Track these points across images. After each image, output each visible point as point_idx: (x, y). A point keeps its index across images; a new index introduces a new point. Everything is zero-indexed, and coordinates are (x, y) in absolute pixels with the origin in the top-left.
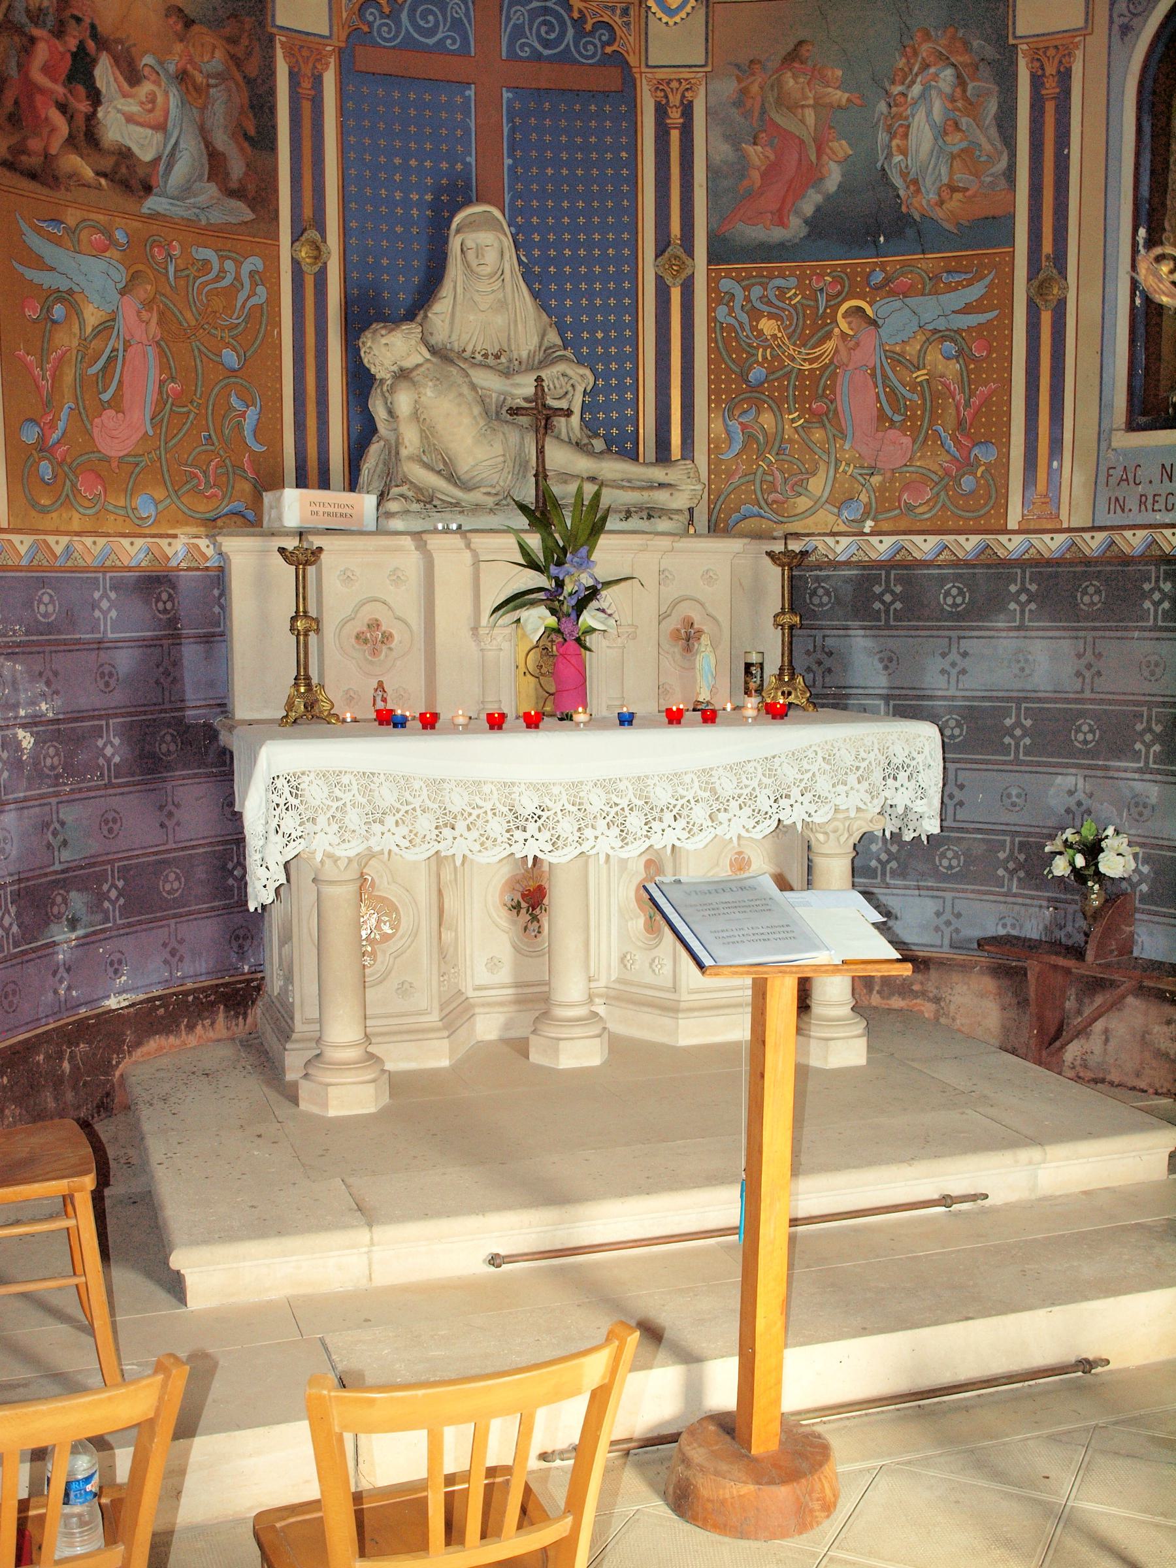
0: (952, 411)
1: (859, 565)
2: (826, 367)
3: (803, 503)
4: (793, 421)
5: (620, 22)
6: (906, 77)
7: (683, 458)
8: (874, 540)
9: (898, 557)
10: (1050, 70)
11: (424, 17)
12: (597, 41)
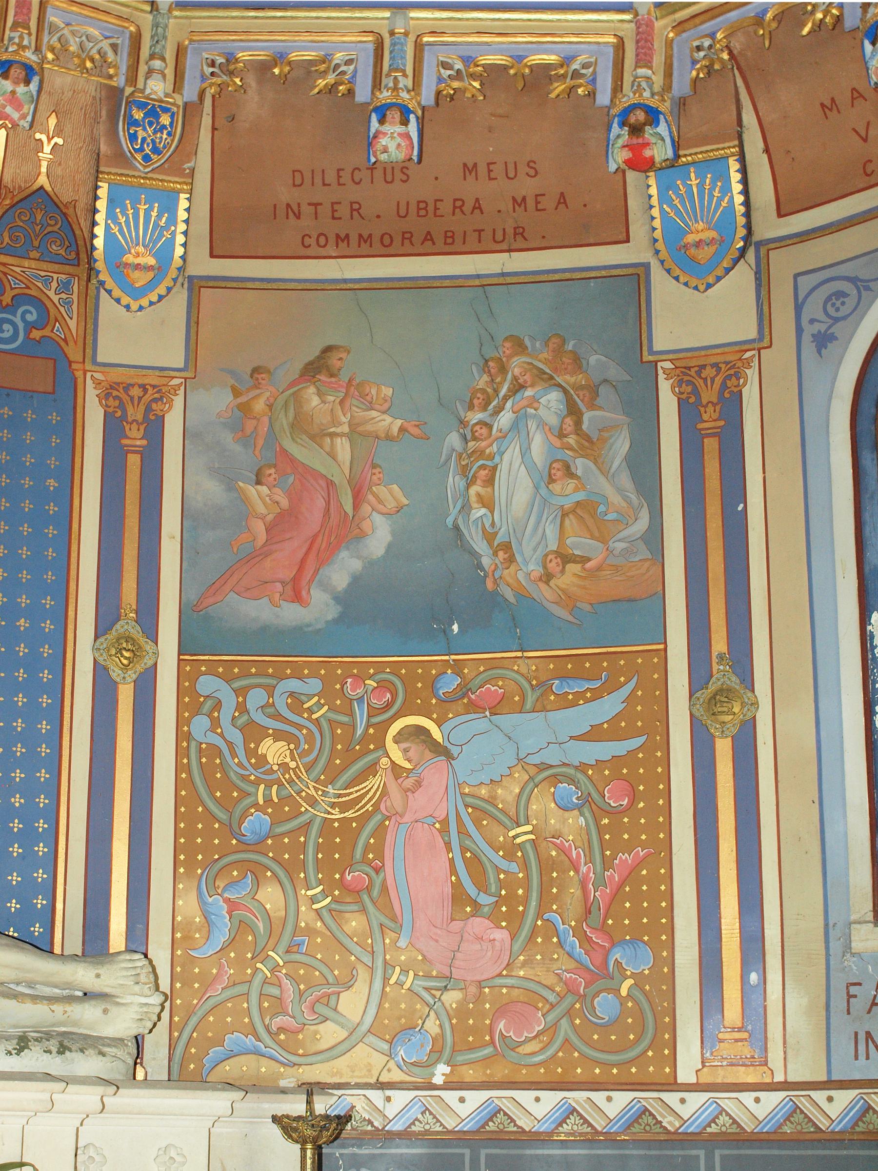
0: (574, 890)
1: (424, 1137)
2: (368, 816)
3: (330, 1033)
4: (313, 900)
5: (55, 299)
6: (486, 400)
7: (129, 950)
8: (451, 1097)
9: (492, 1126)
12: (18, 320)
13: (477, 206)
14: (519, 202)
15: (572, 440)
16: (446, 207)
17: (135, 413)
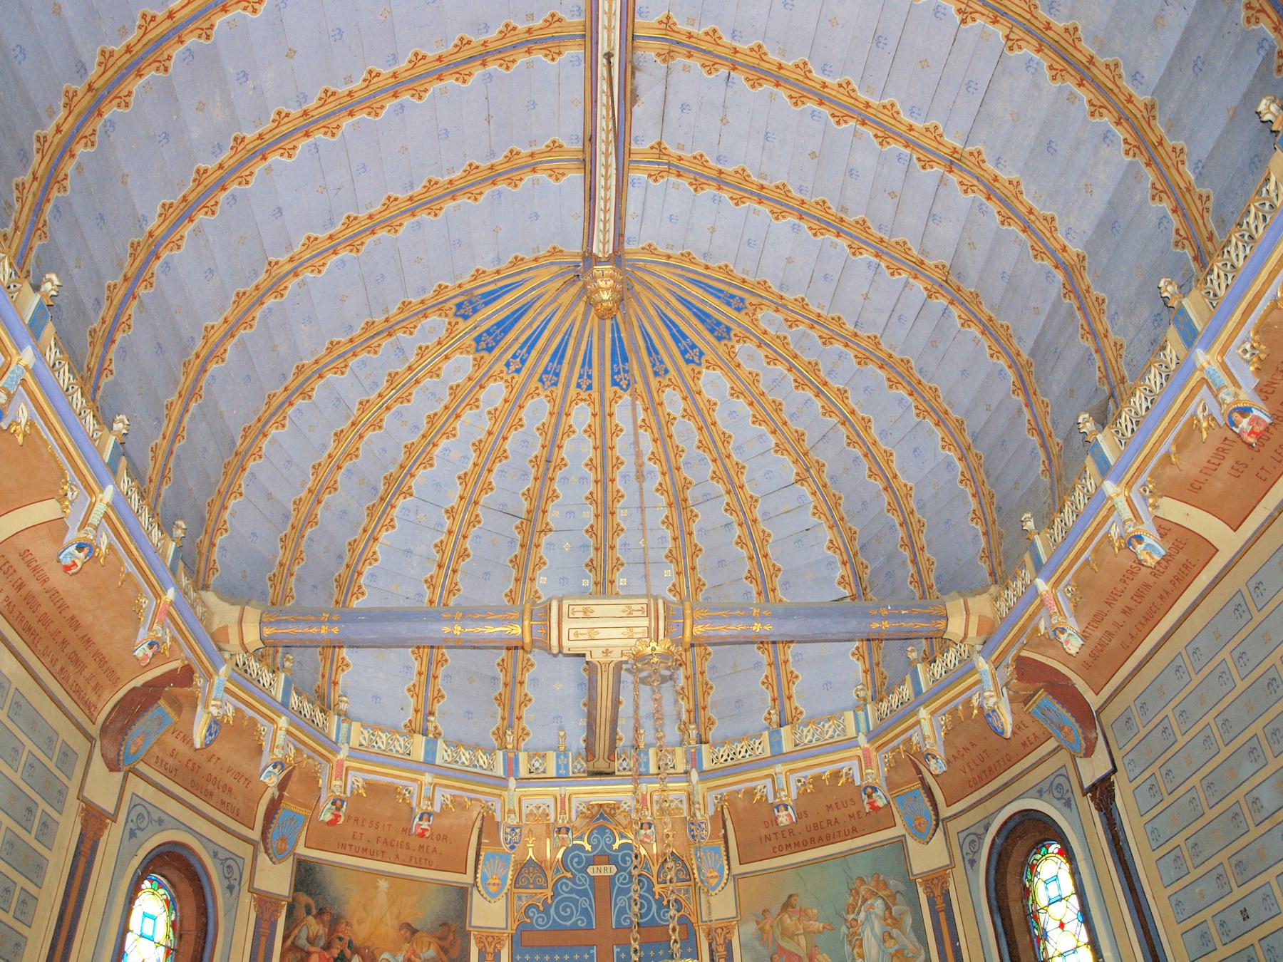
6: (852, 908)
10: (938, 892)
11: (564, 909)
13: (836, 821)
14: (851, 816)
15: (889, 921)
16: (824, 824)
17: (266, 916)
